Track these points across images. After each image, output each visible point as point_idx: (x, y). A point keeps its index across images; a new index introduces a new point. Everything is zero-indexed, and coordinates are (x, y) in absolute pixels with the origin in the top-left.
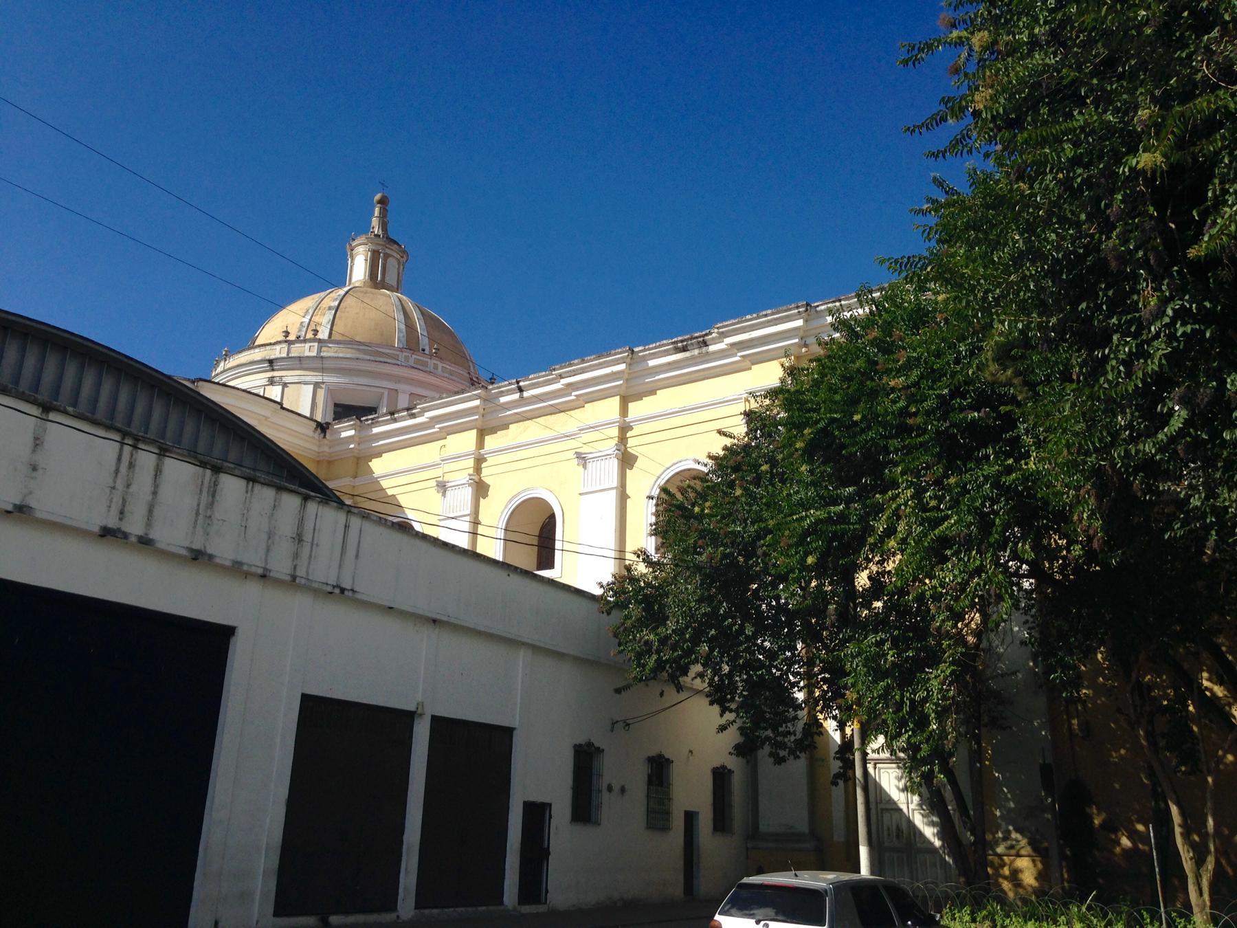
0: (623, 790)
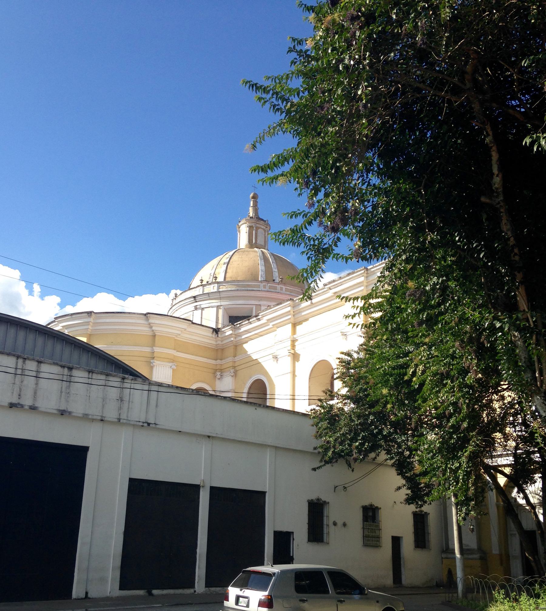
0: (345, 525)
